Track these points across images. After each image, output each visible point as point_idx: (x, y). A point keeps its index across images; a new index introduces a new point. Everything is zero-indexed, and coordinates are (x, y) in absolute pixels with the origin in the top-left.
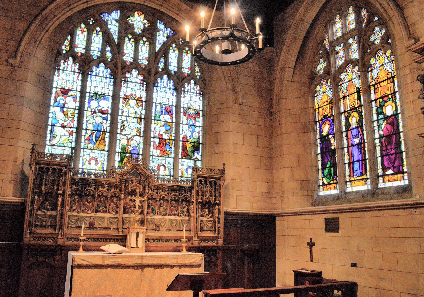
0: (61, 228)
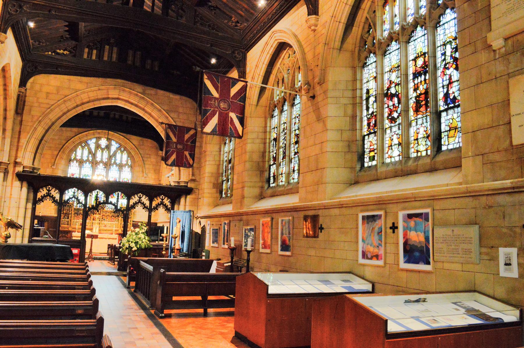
0: (70, 225)
